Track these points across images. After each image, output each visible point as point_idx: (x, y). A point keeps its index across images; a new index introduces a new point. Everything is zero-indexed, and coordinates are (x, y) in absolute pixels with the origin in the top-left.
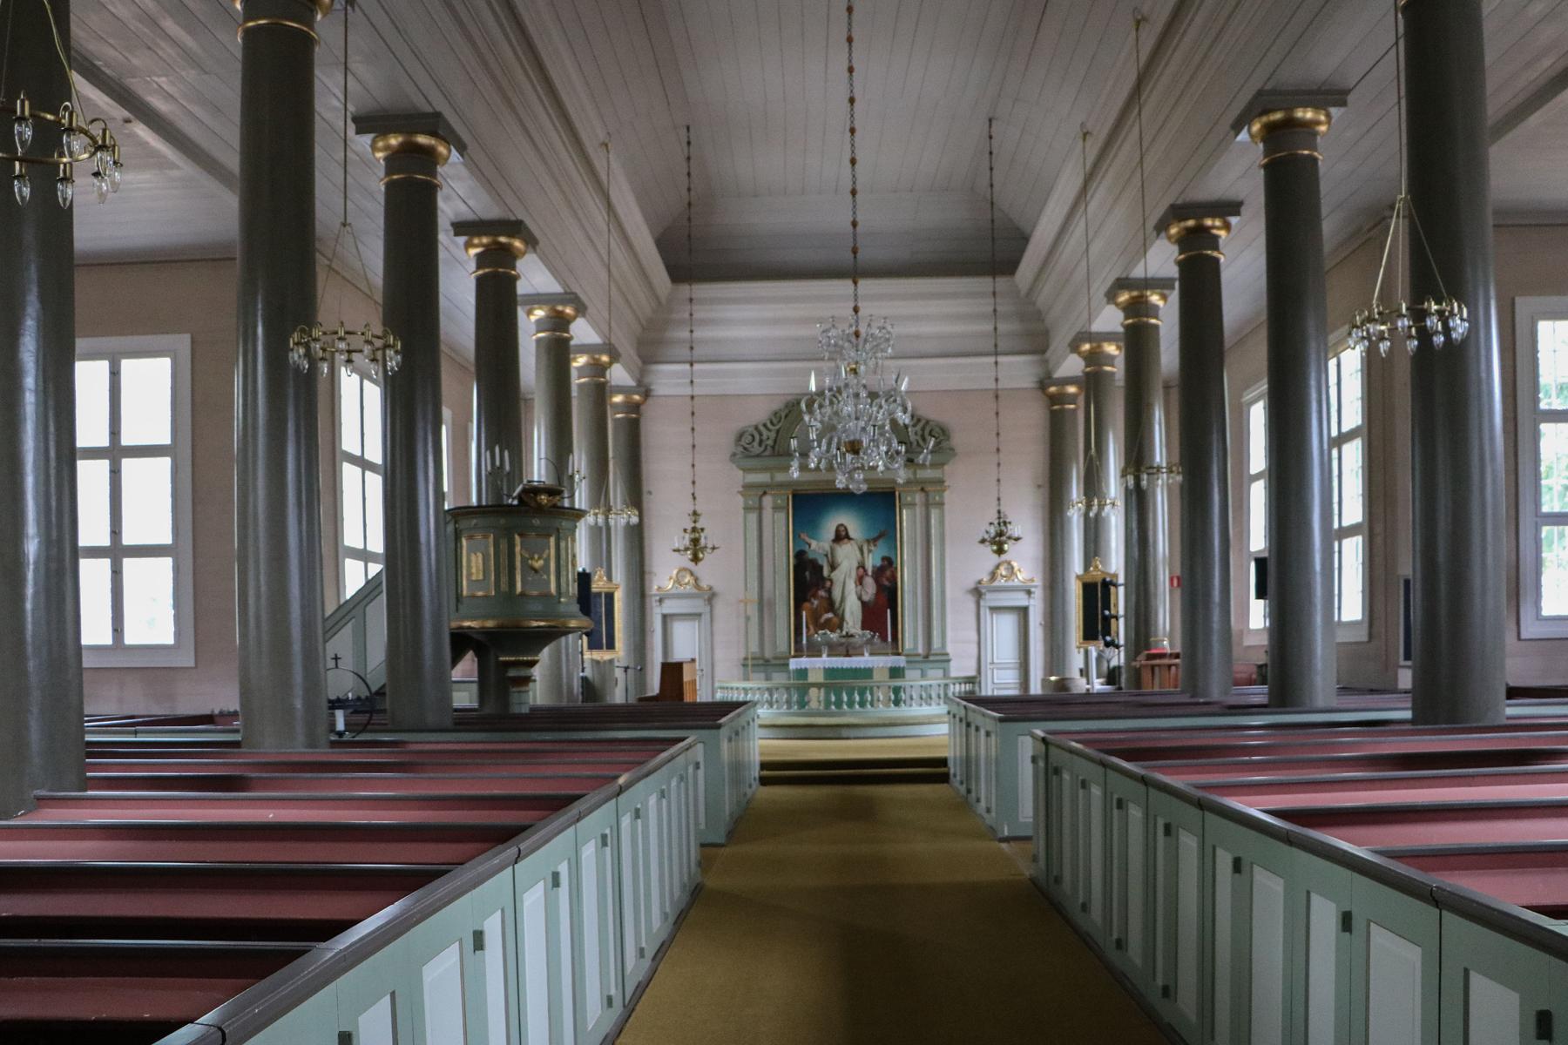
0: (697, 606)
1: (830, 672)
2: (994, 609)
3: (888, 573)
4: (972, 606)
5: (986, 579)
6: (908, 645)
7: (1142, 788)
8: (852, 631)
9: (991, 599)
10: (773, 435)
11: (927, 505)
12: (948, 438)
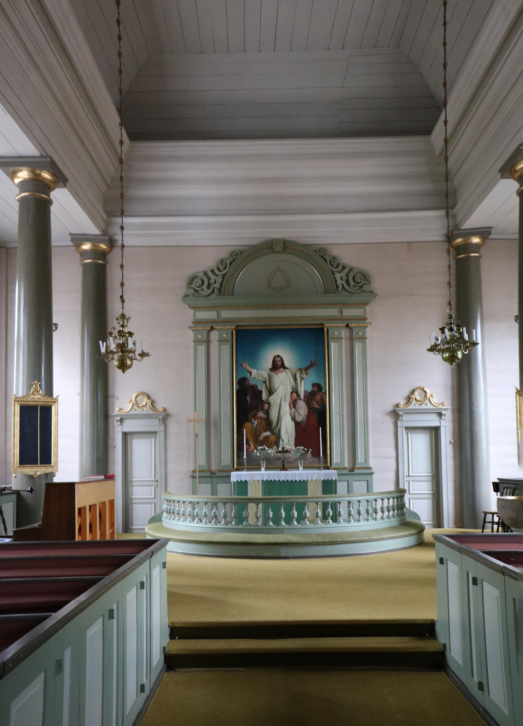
0: (153, 425)
1: (268, 485)
2: (407, 428)
3: (318, 398)
4: (391, 427)
5: (402, 402)
6: (336, 459)
7: (500, 576)
8: (287, 447)
9: (407, 420)
10: (219, 279)
11: (351, 339)
12: (369, 282)
